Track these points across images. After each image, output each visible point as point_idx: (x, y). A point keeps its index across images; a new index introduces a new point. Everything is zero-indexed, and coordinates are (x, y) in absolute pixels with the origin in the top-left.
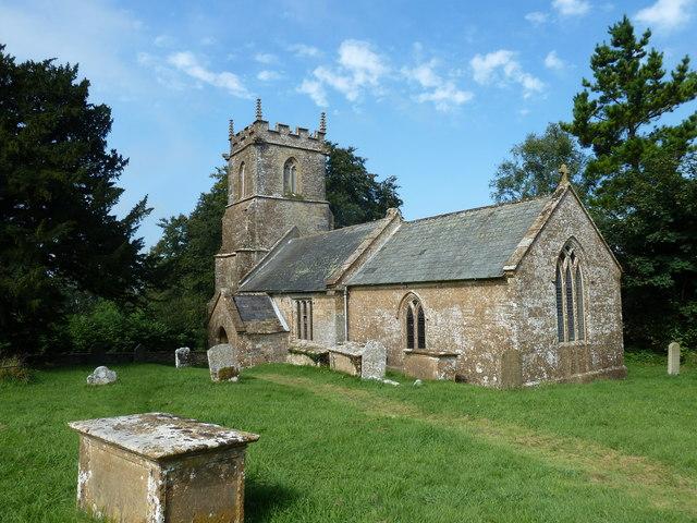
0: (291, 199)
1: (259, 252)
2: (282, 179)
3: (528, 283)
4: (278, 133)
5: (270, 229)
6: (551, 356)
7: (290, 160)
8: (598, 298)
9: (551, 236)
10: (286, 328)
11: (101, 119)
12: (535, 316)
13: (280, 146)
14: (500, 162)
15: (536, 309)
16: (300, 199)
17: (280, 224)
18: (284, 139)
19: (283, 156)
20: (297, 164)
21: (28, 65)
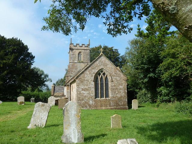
0: (80, 62)
1: (70, 76)
2: (77, 57)
3: (82, 82)
4: (76, 46)
5: (74, 70)
6: (91, 102)
7: (80, 52)
8: (115, 86)
9: (93, 69)
10: (65, 95)
11: (25, 48)
12: (85, 90)
13: (77, 49)
14: (126, 47)
15: (85, 89)
16: (82, 62)
17: (76, 69)
18: (78, 47)
19: (78, 52)
20: (82, 54)
21: (9, 39)
